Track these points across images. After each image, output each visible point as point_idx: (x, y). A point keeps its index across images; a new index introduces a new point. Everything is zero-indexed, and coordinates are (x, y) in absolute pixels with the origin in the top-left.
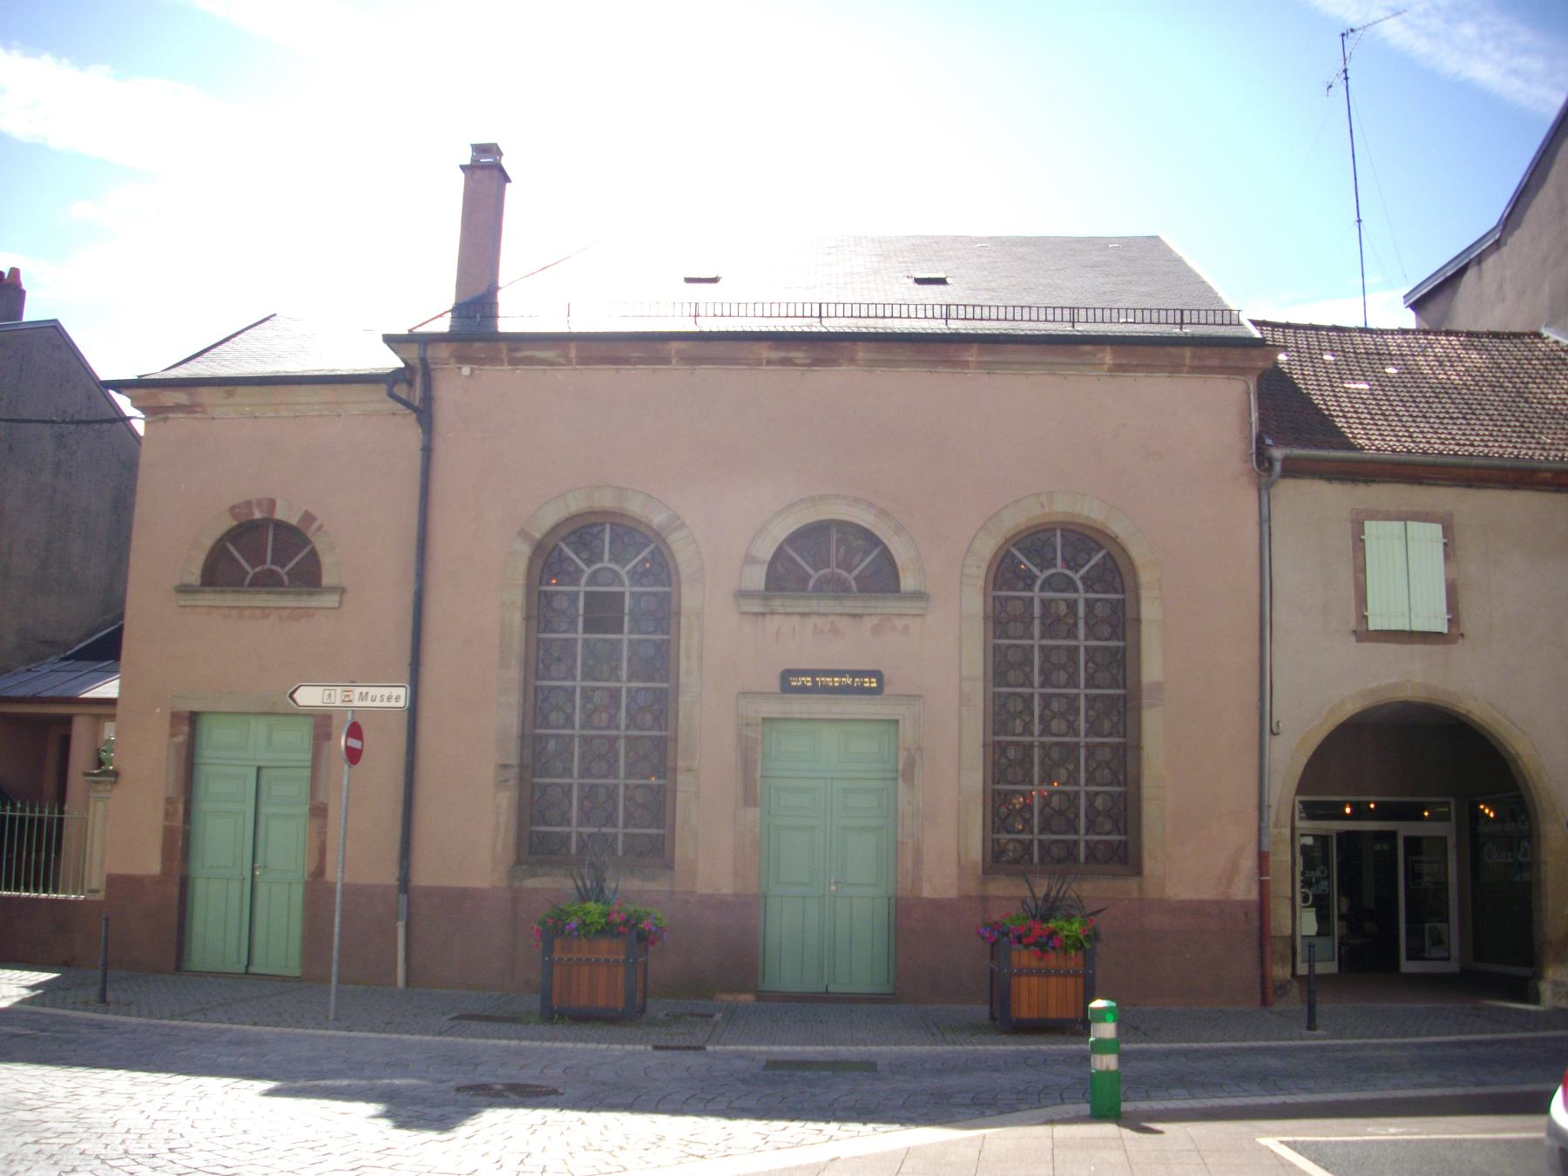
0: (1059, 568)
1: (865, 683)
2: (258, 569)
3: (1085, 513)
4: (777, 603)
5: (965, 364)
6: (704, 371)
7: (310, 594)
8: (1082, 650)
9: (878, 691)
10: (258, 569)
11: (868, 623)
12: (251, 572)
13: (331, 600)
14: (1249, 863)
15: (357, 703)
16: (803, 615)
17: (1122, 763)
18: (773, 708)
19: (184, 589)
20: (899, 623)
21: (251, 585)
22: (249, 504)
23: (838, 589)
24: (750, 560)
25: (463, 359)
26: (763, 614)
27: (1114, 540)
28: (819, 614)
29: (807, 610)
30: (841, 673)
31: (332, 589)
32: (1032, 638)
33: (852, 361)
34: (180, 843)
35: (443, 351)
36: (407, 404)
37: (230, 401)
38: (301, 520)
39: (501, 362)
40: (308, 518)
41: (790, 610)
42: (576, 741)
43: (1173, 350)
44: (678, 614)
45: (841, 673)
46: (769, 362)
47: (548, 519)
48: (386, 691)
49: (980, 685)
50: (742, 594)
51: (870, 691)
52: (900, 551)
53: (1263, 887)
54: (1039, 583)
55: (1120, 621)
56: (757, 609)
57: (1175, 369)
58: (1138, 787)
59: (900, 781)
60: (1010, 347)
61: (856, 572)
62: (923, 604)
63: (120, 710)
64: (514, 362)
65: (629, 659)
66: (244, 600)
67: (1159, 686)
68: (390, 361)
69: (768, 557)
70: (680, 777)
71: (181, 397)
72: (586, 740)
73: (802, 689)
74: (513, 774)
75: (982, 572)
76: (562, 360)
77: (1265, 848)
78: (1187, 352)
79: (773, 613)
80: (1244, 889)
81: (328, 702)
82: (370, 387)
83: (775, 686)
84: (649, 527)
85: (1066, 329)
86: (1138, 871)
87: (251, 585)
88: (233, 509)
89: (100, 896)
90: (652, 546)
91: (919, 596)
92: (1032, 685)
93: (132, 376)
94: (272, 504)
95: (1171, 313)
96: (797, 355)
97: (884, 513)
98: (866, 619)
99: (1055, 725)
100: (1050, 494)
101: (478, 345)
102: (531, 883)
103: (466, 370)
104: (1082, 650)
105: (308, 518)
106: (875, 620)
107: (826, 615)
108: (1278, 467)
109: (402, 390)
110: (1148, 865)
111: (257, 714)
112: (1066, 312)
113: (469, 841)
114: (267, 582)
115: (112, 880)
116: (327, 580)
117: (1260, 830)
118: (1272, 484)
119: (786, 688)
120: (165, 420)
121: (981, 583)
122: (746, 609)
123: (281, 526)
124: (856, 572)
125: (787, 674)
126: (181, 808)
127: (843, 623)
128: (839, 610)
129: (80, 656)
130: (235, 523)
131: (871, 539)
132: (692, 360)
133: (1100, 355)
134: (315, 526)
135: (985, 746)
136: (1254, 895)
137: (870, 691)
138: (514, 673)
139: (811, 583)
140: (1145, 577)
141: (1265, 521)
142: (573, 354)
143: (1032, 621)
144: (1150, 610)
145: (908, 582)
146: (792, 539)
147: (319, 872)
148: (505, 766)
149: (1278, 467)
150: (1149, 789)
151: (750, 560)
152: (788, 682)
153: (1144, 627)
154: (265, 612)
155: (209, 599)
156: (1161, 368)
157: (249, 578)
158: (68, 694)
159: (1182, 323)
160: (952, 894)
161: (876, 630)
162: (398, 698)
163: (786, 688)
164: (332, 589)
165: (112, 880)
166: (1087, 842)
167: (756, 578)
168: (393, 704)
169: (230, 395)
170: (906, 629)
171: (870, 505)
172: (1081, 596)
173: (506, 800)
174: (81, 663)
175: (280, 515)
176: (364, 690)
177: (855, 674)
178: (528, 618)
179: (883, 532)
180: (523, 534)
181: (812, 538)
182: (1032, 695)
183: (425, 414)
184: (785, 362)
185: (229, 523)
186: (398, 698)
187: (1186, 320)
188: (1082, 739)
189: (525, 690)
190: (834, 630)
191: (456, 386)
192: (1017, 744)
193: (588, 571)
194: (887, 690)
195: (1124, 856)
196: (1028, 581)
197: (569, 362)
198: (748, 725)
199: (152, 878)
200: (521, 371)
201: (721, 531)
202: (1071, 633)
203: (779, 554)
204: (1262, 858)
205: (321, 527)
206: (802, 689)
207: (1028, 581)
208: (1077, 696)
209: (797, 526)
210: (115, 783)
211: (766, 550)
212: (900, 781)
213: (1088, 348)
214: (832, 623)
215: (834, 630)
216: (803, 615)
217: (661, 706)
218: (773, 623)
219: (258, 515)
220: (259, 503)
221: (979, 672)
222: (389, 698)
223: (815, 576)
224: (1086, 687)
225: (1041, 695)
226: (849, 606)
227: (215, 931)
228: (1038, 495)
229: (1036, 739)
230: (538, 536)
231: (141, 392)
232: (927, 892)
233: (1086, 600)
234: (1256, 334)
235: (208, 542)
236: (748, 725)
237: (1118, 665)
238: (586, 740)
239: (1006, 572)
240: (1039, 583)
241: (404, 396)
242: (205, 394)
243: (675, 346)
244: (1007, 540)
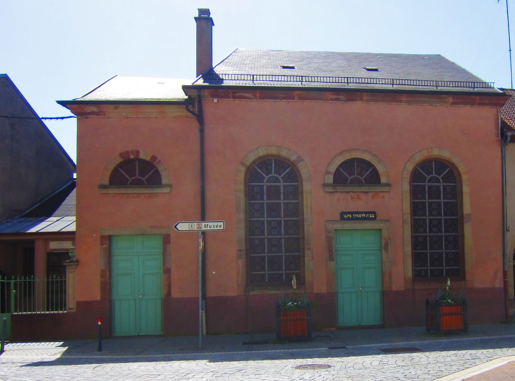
0: (434, 175)
1: (371, 216)
2: (133, 178)
3: (444, 155)
4: (338, 189)
5: (401, 101)
6: (306, 103)
7: (158, 187)
8: (442, 203)
9: (374, 219)
10: (133, 178)
11: (371, 195)
12: (130, 179)
13: (167, 190)
14: (500, 275)
15: (203, 228)
16: (347, 192)
17: (457, 242)
18: (338, 226)
19: (102, 187)
20: (381, 195)
21: (130, 184)
22: (128, 152)
23: (359, 183)
24: (328, 173)
25: (214, 96)
26: (333, 192)
27: (453, 164)
28: (353, 192)
29: (349, 190)
30: (361, 213)
31: (166, 186)
32: (425, 199)
33: (361, 100)
34: (107, 286)
35: (206, 93)
36: (193, 113)
37: (116, 111)
38: (151, 158)
39: (229, 98)
40: (154, 158)
41: (342, 190)
42: (266, 240)
43: (473, 97)
44: (302, 193)
45: (361, 213)
46: (331, 100)
47: (252, 158)
48: (215, 224)
49: (410, 216)
50: (325, 185)
51: (372, 219)
52: (380, 169)
53: (506, 283)
54: (427, 180)
55: (456, 193)
56: (331, 190)
57: (473, 104)
58: (463, 249)
59: (383, 251)
60: (417, 95)
61: (364, 177)
62: (389, 188)
63: (77, 236)
64: (234, 97)
65: (284, 209)
66: (130, 191)
67: (469, 215)
68: (182, 96)
69: (334, 172)
70: (306, 252)
71: (94, 109)
72: (269, 240)
73: (348, 219)
74: (244, 253)
75: (409, 176)
76: (253, 97)
77: (506, 270)
78: (478, 98)
79: (336, 192)
80: (499, 284)
81: (191, 229)
82: (175, 106)
83: (338, 217)
84: (290, 161)
85: (434, 89)
86: (464, 278)
87: (130, 184)
88: (121, 155)
89: (74, 311)
90: (291, 168)
91: (388, 185)
92: (426, 216)
93: (70, 99)
94: (138, 152)
95: (470, 83)
96: (342, 97)
97: (374, 155)
98: (369, 193)
99: (434, 229)
100: (432, 148)
101: (220, 90)
102: (252, 293)
103: (215, 100)
104: (442, 203)
105: (154, 158)
106: (372, 194)
107: (356, 192)
108: (509, 138)
109: (191, 108)
110: (468, 276)
111: (137, 235)
112: (434, 82)
113: (229, 277)
114: (138, 183)
115: (79, 304)
116: (164, 181)
117: (504, 263)
118: (507, 145)
119: (342, 219)
120: (87, 118)
121: (409, 180)
122: (327, 191)
123: (143, 162)
124: (364, 177)
125: (342, 214)
126: (108, 273)
127: (362, 196)
128: (360, 190)
129: (28, 215)
130: (122, 160)
131: (369, 164)
132: (302, 98)
133: (448, 99)
134: (157, 161)
135: (411, 237)
136: (502, 286)
137: (372, 219)
138: (242, 216)
139: (349, 181)
140: (464, 177)
141: (503, 159)
142: (258, 95)
143: (425, 193)
144: (466, 189)
145: (383, 180)
146: (341, 166)
147: (169, 294)
148: (240, 250)
149: (509, 138)
150: (467, 249)
151: (328, 173)
152: (343, 217)
153: (464, 195)
154: (138, 195)
155: (113, 191)
156: (468, 104)
157: (129, 182)
158: (22, 231)
159: (474, 87)
160: (403, 289)
161: (373, 197)
162: (220, 226)
163: (342, 219)
164: (166, 186)
165: (79, 304)
166: (446, 269)
167: (330, 179)
168: (218, 228)
169: (116, 108)
170: (383, 197)
171: (370, 152)
172: (441, 184)
173: (241, 263)
174: (30, 219)
175: (142, 156)
176: (206, 223)
177: (366, 213)
178: (246, 195)
179: (374, 162)
180: (242, 163)
181: (347, 165)
182: (426, 219)
183: (200, 118)
184: (338, 100)
185: (120, 160)
186: (220, 226)
187: (476, 86)
188: (443, 234)
189: (246, 222)
190: (358, 197)
191: (212, 106)
192: (421, 236)
193: (267, 177)
194: (378, 218)
195: (458, 273)
196: (423, 179)
197: (256, 99)
198: (329, 232)
199: (97, 301)
200: (237, 101)
201: (315, 172)
202: (439, 198)
203: (337, 170)
204: (505, 273)
205: (160, 161)
206: (348, 219)
207: (423, 179)
208: (441, 219)
209: (344, 160)
210: (77, 265)
211: (333, 169)
212: (383, 251)
213: (444, 96)
214: (358, 195)
215: (358, 197)
216: (347, 192)
217: (297, 225)
218: (337, 196)
219: (132, 157)
220: (132, 152)
221: (409, 211)
222: (217, 226)
223: (350, 178)
224: (444, 216)
225: (429, 219)
226: (364, 189)
227: (125, 319)
228: (427, 149)
229: (428, 234)
230: (248, 164)
231: (76, 106)
232: (394, 288)
233: (443, 185)
234: (501, 92)
235: (111, 168)
236: (329, 232)
237: (455, 209)
238: (269, 240)
239: (416, 176)
240: (427, 180)
241: (192, 110)
242: (104, 107)
243: (297, 92)
244: (417, 165)
